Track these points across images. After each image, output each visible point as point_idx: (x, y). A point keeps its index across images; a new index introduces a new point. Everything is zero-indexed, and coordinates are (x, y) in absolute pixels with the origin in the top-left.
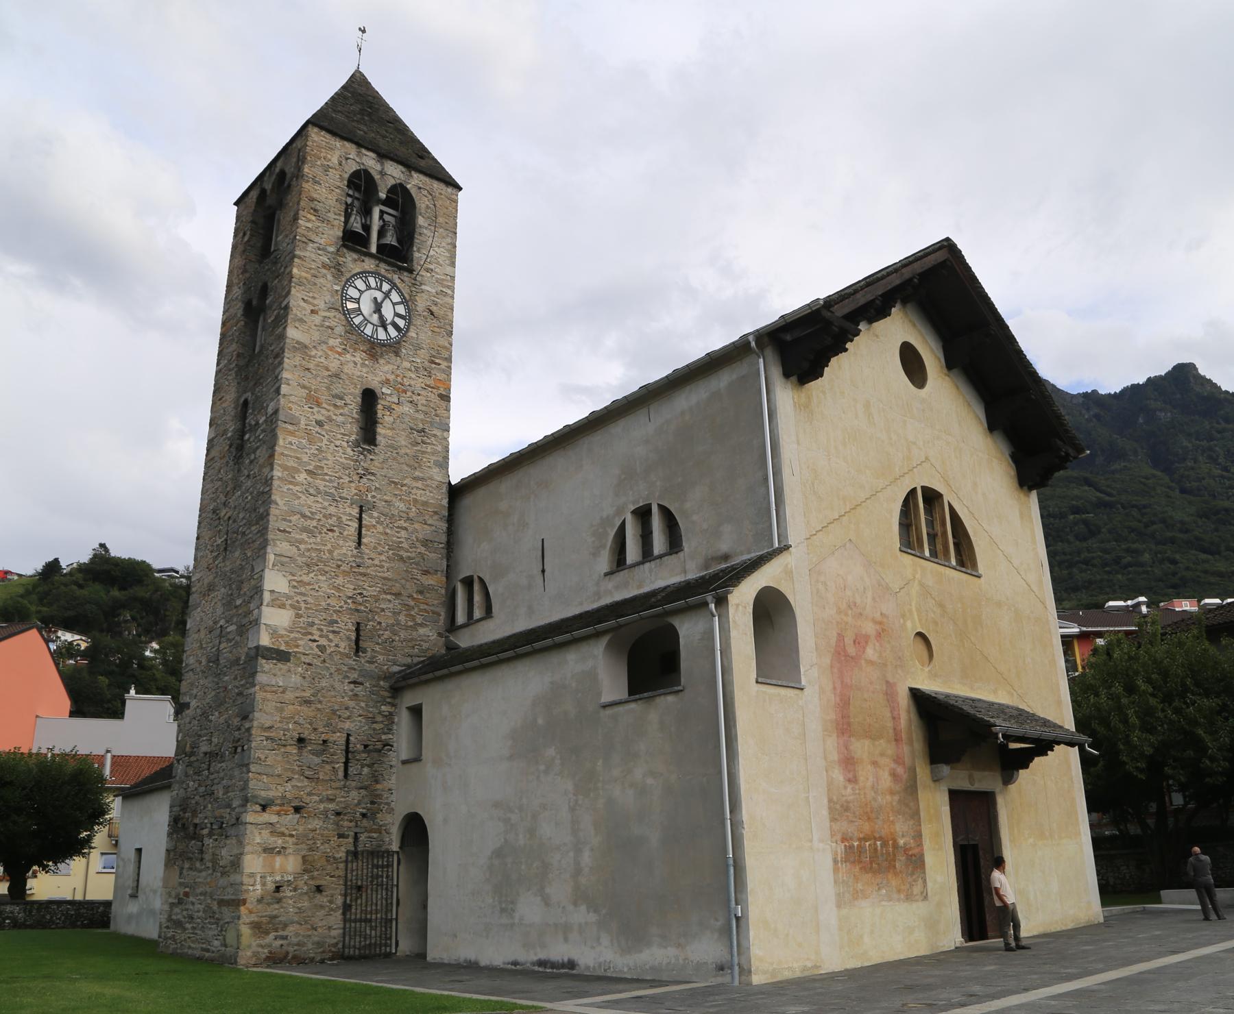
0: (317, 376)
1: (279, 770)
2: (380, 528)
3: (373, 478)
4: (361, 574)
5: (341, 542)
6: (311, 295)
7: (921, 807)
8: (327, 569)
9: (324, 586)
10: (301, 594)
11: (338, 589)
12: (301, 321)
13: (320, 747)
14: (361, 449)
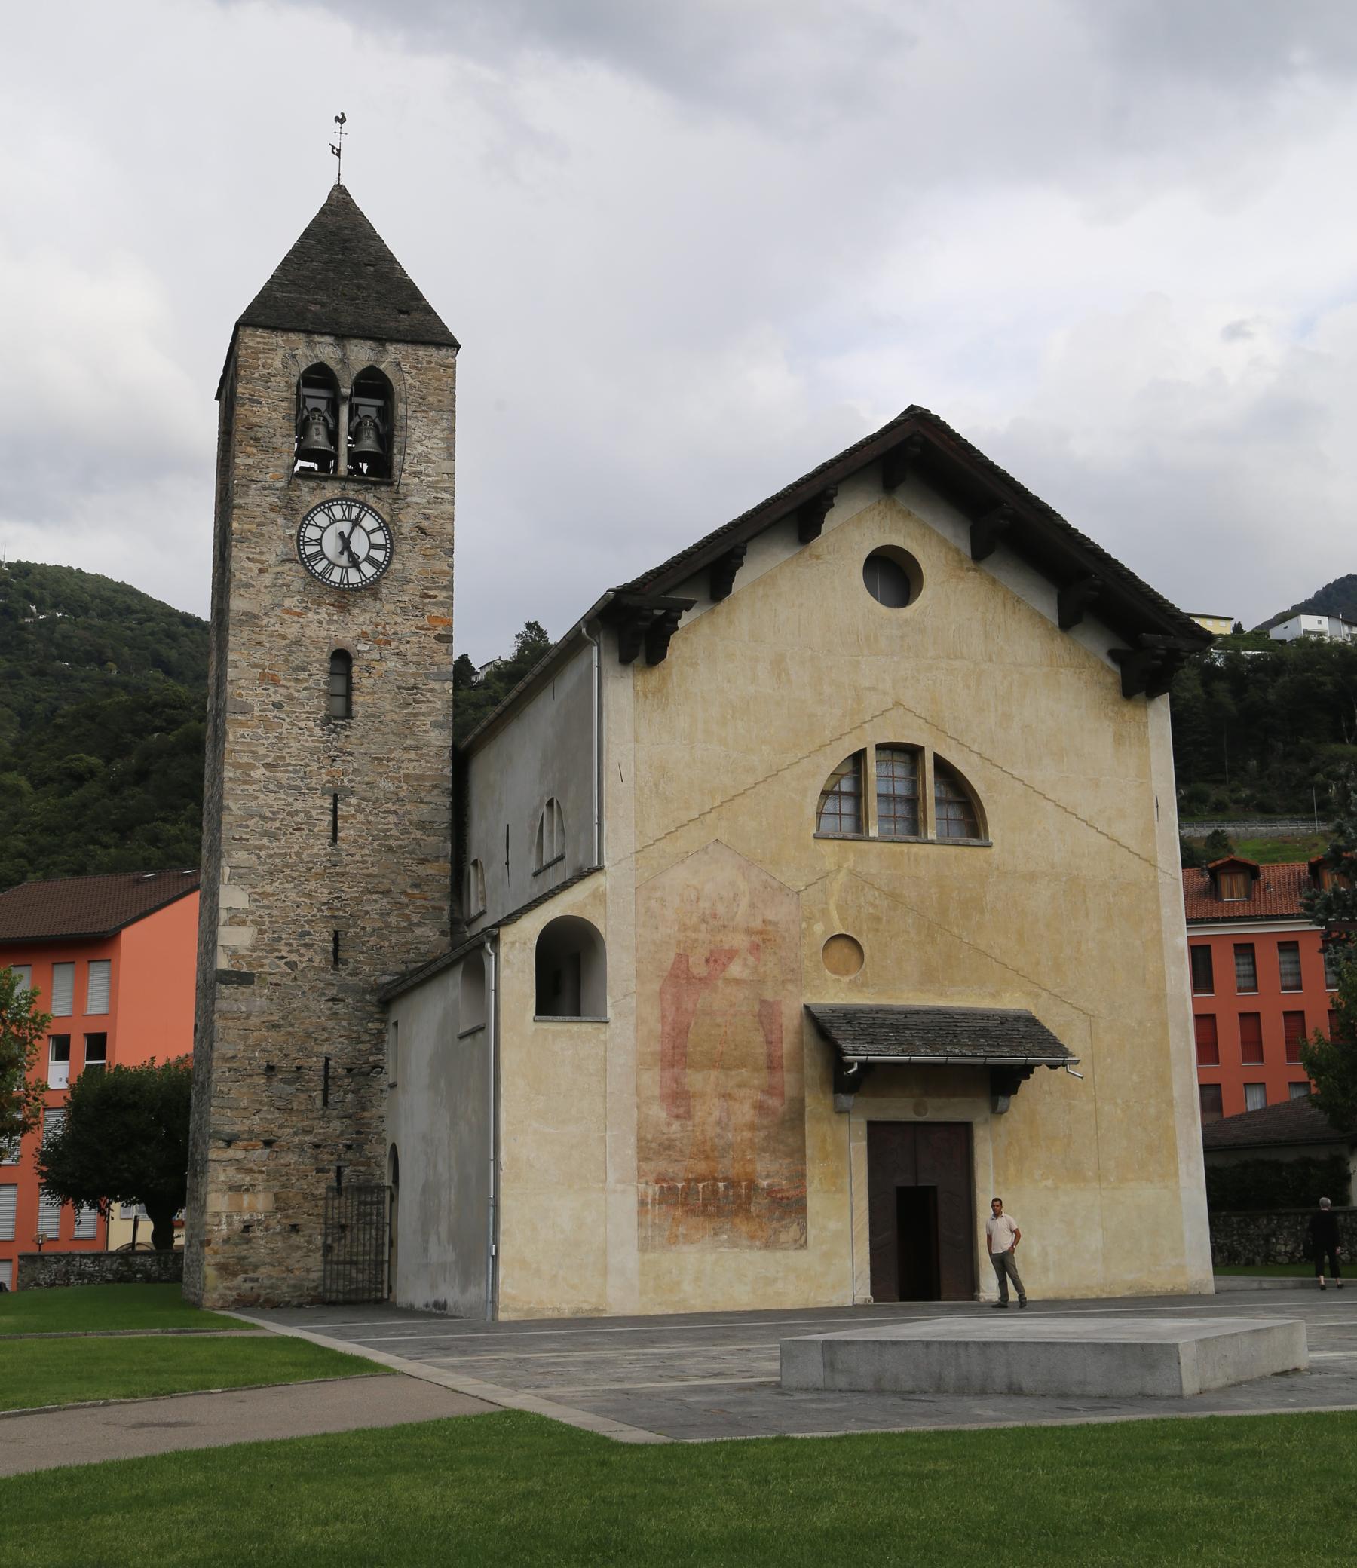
0: (271, 649)
1: (244, 1103)
2: (361, 817)
3: (349, 758)
4: (338, 874)
5: (311, 841)
6: (258, 550)
8: (294, 874)
11: (309, 896)
12: (248, 586)
14: (332, 726)
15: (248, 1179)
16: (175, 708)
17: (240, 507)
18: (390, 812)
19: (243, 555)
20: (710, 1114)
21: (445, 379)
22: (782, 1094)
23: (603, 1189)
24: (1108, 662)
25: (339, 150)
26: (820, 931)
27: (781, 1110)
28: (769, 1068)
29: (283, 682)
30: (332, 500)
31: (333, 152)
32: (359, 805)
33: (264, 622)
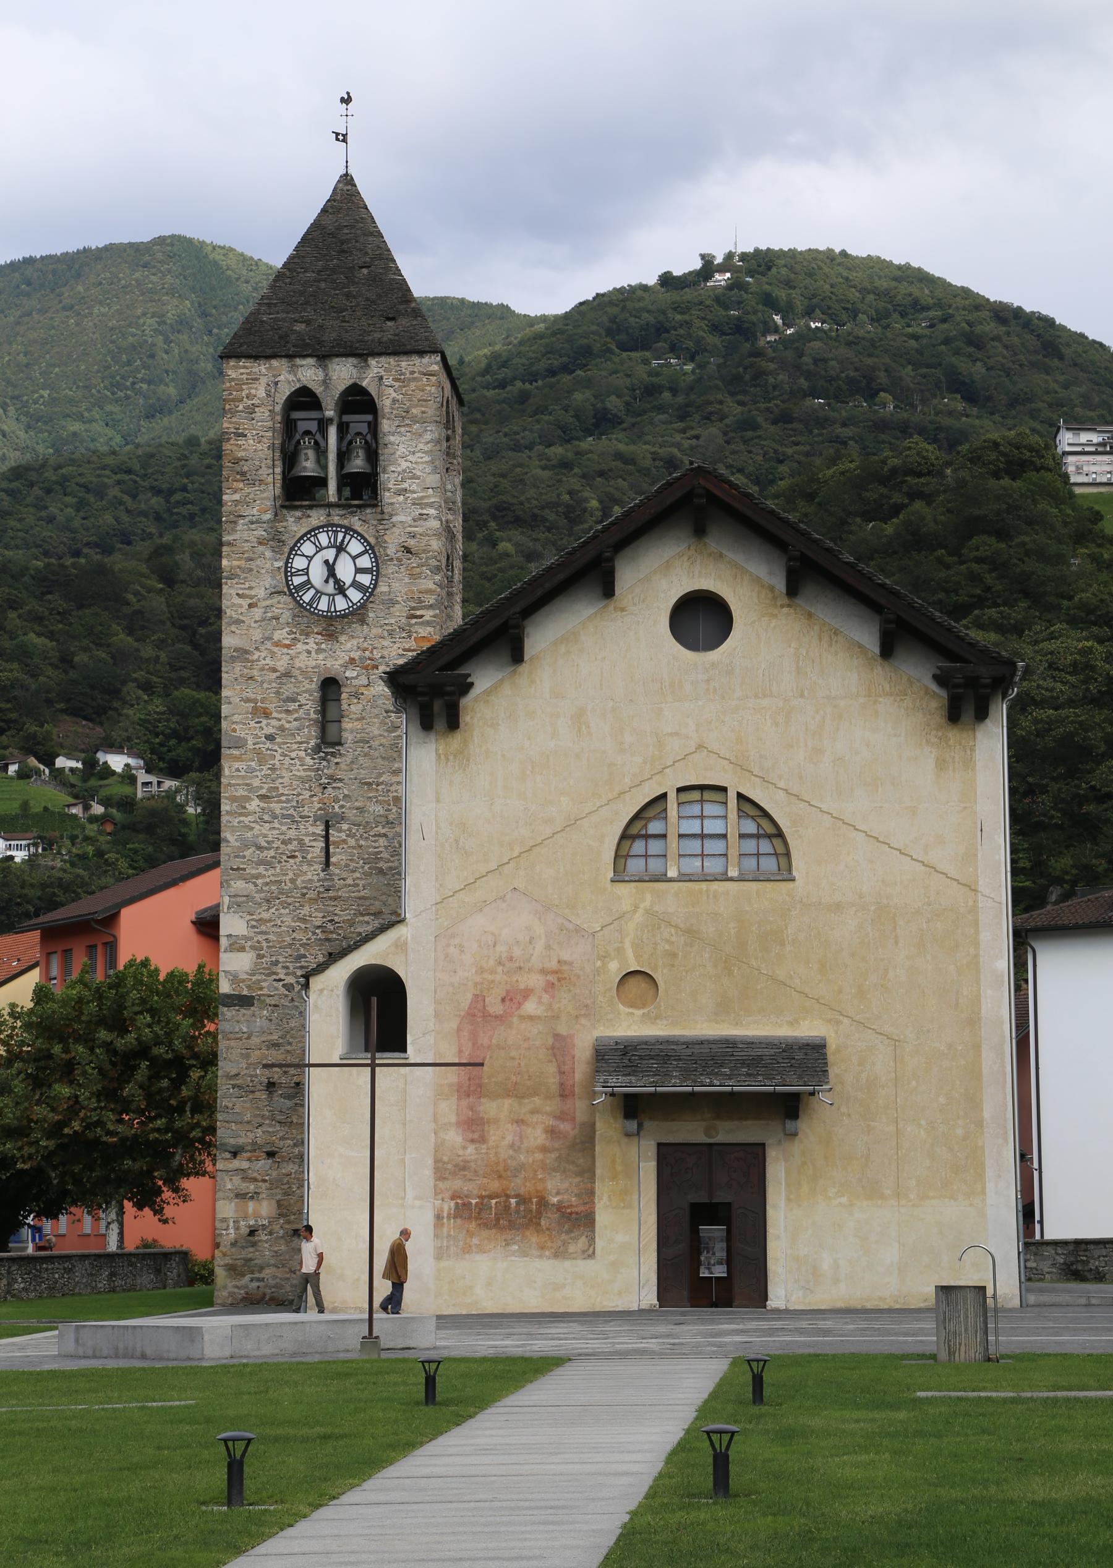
0: (262, 682)
1: (248, 1117)
2: (352, 842)
3: (339, 785)
4: (331, 898)
5: (305, 868)
6: (247, 586)
7: (597, 1164)
8: (290, 900)
9: (288, 920)
10: (261, 933)
11: (303, 920)
12: (238, 622)
13: (292, 1090)
14: (322, 754)
15: (252, 1187)
16: (920, 475)
17: (229, 544)
18: (380, 835)
19: (233, 592)
20: (503, 1138)
21: (428, 388)
22: (573, 1119)
23: (403, 1206)
24: (934, 687)
25: (345, 136)
26: (615, 969)
27: (572, 1133)
28: (561, 1096)
29: (275, 715)
30: (318, 528)
31: (337, 139)
32: (350, 830)
33: (255, 657)
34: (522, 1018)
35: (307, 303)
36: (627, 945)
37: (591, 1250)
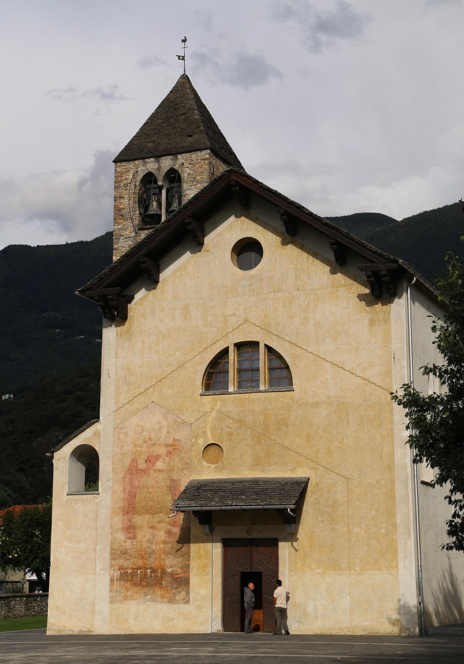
17: (116, 249)
20: (145, 536)
21: (204, 166)
23: (94, 573)
26: (202, 443)
31: (179, 59)
34: (155, 471)
35: (155, 134)
36: (208, 430)
37: (188, 598)
